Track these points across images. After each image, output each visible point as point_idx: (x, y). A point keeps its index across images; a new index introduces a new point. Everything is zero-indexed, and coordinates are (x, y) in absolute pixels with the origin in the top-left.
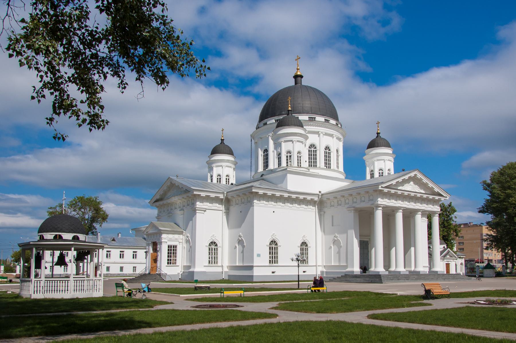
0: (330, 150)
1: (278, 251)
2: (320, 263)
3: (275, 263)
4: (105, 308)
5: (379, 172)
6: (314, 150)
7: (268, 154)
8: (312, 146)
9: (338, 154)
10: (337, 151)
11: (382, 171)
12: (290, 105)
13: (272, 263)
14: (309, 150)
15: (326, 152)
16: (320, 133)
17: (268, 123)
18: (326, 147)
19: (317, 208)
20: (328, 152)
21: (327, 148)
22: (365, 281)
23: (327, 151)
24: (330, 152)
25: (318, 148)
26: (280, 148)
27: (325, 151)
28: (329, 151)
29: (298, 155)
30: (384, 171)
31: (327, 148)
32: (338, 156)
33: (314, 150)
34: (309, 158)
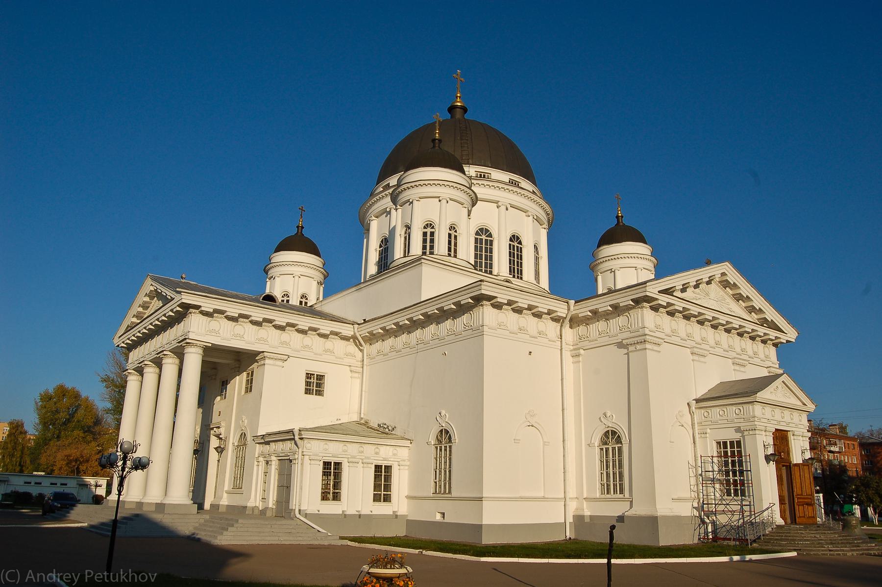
0: (520, 243)
1: (508, 258)
2: (572, 493)
3: (608, 494)
4: (840, 537)
5: (425, 230)
6: (486, 240)
7: (388, 247)
8: (483, 231)
9: (538, 253)
10: (536, 247)
11: (433, 228)
12: (439, 130)
13: (615, 492)
14: (476, 239)
15: (514, 246)
16: (500, 204)
17: (674, 294)
18: (514, 236)
19: (208, 304)
20: (517, 247)
21: (515, 238)
22: (853, 547)
23: (516, 244)
24: (521, 248)
25: (495, 235)
26: (389, 215)
27: (510, 245)
28: (520, 246)
29: (450, 232)
30: (436, 227)
31: (515, 238)
32: (537, 259)
33: (486, 240)
34: (476, 255)
